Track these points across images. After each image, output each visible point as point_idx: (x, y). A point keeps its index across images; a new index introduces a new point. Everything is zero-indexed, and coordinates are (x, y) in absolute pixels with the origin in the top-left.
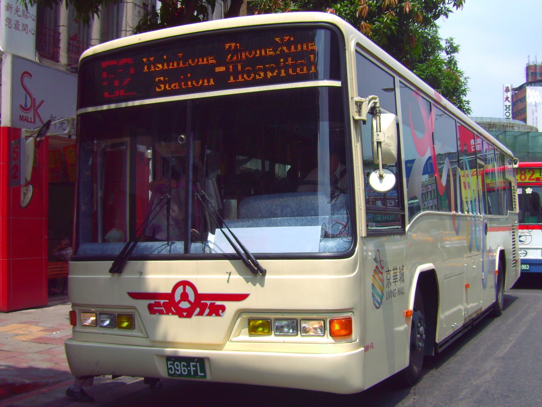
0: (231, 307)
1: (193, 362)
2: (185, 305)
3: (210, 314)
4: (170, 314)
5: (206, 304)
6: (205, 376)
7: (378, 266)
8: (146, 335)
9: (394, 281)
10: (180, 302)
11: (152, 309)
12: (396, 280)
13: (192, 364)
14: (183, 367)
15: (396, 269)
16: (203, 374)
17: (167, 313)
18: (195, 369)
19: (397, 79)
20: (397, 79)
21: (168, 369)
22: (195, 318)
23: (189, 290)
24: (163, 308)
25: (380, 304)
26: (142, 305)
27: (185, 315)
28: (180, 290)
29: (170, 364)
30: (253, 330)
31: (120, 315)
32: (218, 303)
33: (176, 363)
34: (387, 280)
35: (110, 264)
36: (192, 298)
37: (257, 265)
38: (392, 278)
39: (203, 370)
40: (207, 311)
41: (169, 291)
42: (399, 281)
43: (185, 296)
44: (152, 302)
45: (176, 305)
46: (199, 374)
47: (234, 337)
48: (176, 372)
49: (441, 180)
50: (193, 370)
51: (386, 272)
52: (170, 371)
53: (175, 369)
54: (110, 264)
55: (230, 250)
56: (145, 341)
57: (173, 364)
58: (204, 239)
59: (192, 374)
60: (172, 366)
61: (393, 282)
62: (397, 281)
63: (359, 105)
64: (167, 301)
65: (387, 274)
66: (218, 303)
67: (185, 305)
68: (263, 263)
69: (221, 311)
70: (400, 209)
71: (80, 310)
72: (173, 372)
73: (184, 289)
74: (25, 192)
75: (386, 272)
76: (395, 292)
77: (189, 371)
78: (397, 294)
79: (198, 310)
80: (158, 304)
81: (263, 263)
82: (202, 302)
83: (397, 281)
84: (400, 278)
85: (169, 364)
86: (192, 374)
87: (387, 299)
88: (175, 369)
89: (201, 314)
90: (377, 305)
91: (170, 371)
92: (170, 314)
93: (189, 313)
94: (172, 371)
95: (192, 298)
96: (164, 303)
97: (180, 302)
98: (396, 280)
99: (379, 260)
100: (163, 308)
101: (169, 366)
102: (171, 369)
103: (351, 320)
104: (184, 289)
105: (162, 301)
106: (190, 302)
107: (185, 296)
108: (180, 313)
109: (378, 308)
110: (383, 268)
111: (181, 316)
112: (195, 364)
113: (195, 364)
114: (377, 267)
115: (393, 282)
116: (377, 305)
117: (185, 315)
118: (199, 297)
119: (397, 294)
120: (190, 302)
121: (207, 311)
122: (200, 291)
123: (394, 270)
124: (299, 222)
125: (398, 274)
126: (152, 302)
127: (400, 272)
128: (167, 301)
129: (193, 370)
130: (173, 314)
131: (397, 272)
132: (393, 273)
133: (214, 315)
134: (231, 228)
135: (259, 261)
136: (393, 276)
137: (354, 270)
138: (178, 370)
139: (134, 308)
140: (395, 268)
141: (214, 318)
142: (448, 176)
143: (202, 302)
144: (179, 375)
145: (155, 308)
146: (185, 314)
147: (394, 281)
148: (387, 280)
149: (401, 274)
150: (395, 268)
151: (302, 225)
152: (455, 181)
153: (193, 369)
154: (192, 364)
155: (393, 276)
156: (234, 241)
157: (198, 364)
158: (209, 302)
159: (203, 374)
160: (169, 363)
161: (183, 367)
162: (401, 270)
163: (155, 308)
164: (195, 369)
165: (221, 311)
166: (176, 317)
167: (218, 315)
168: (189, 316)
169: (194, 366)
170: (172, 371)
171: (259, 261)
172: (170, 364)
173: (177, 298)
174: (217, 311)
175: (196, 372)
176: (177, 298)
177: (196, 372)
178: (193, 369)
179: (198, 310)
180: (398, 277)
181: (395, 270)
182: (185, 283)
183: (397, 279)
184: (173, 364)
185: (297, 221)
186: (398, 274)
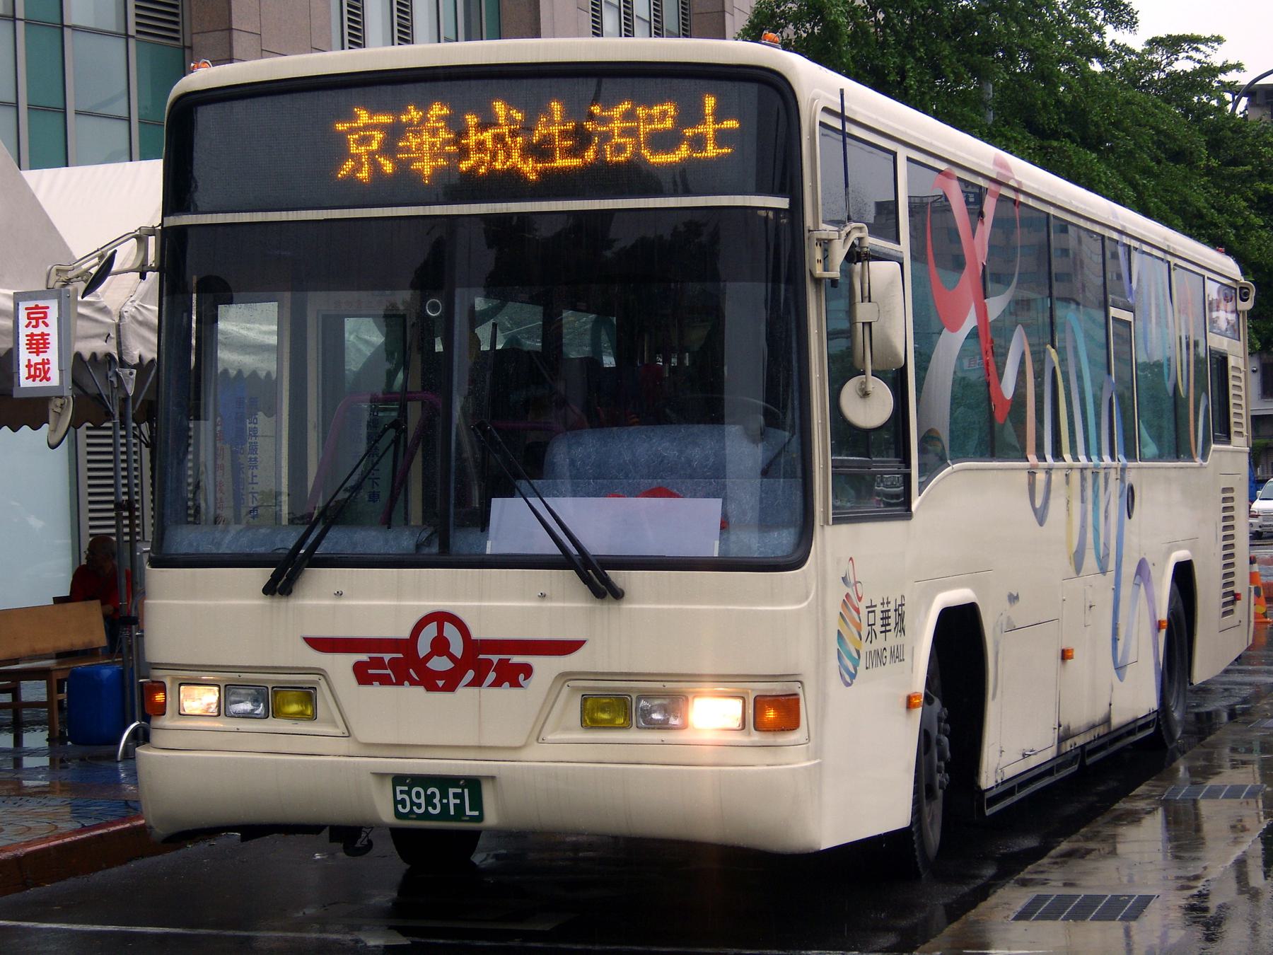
0: (545, 667)
1: (457, 786)
2: (440, 664)
3: (497, 683)
4: (406, 683)
5: (490, 662)
6: (480, 818)
7: (851, 594)
8: (346, 731)
9: (883, 629)
10: (428, 657)
11: (363, 675)
12: (888, 628)
13: (451, 791)
14: (420, 804)
15: (888, 603)
16: (476, 813)
17: (400, 683)
18: (458, 801)
19: (903, 153)
20: (903, 153)
21: (396, 802)
22: (464, 693)
23: (450, 631)
24: (389, 671)
25: (853, 676)
26: (341, 665)
27: (440, 686)
28: (430, 631)
29: (402, 792)
30: (590, 721)
31: (279, 689)
32: (516, 659)
33: (415, 790)
34: (869, 625)
35: (262, 575)
36: (457, 648)
37: (606, 581)
38: (879, 622)
39: (477, 803)
40: (492, 676)
41: (405, 634)
42: (893, 630)
43: (440, 646)
44: (364, 657)
45: (420, 664)
46: (468, 812)
47: (554, 731)
48: (415, 808)
49: (1001, 382)
50: (455, 805)
51: (867, 607)
52: (400, 807)
53: (412, 803)
54: (262, 575)
55: (547, 547)
56: (344, 745)
57: (409, 793)
58: (482, 521)
59: (452, 813)
60: (405, 797)
61: (881, 632)
62: (890, 631)
63: (826, 244)
64: (400, 655)
65: (869, 612)
66: (516, 659)
67: (440, 664)
68: (617, 576)
69: (521, 677)
70: (900, 462)
71: (174, 679)
72: (407, 809)
73: (440, 629)
74: (58, 410)
75: (867, 607)
76: (885, 654)
77: (445, 807)
78: (888, 658)
79: (470, 674)
80: (378, 663)
81: (617, 576)
82: (481, 656)
83: (890, 631)
84: (897, 624)
85: (398, 793)
86: (452, 813)
87: (867, 668)
88: (412, 803)
89: (477, 682)
90: (848, 680)
91: (400, 807)
92: (406, 683)
93: (450, 682)
94: (404, 807)
95: (457, 648)
96: (392, 660)
97: (428, 657)
98: (888, 628)
99: (852, 581)
100: (389, 671)
101: (399, 797)
102: (403, 802)
103: (797, 701)
104: (440, 629)
105: (387, 657)
106: (452, 657)
107: (440, 646)
108: (429, 681)
109: (848, 685)
110: (860, 599)
111: (431, 687)
112: (459, 790)
113: (459, 790)
114: (847, 596)
115: (881, 632)
116: (848, 680)
117: (440, 686)
118: (474, 647)
119: (888, 658)
120: (452, 657)
121: (492, 676)
122: (476, 634)
123: (883, 604)
124: (703, 487)
125: (892, 614)
126: (364, 657)
127: (896, 610)
128: (400, 655)
129: (455, 805)
130: (413, 683)
131: (889, 611)
132: (882, 612)
133: (507, 684)
134: (547, 496)
135: (611, 574)
136: (882, 619)
137: (801, 602)
138: (419, 806)
139: (320, 672)
140: (885, 601)
141: (506, 691)
142: (1021, 373)
143: (481, 656)
144: (420, 817)
145: (370, 671)
146: (440, 683)
147: (883, 629)
148: (869, 625)
149: (899, 615)
150: (885, 601)
151: (588, 495)
152: (1039, 375)
153: (453, 801)
154: (451, 791)
155: (882, 619)
156: (557, 529)
157: (466, 791)
158: (495, 658)
159: (476, 813)
160: (398, 789)
161: (420, 804)
162: (899, 605)
163: (370, 671)
164: (458, 801)
165: (521, 677)
166: (420, 690)
167: (515, 684)
168: (451, 687)
169: (456, 796)
170: (404, 807)
171: (611, 574)
172: (402, 792)
173: (423, 648)
174: (512, 676)
175: (460, 808)
176: (423, 648)
177: (460, 808)
178: (453, 801)
179: (470, 674)
180: (892, 621)
181: (885, 605)
182: (441, 618)
183: (889, 624)
184: (409, 793)
185: (578, 487)
186: (892, 614)
